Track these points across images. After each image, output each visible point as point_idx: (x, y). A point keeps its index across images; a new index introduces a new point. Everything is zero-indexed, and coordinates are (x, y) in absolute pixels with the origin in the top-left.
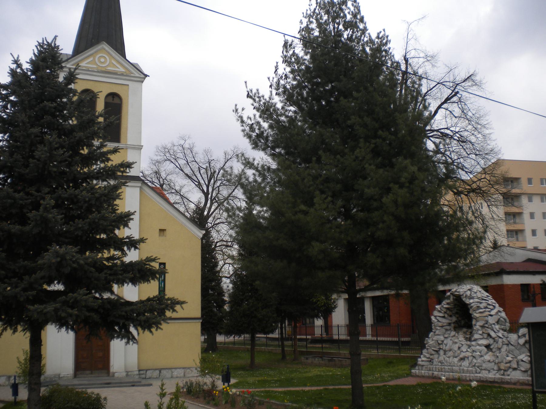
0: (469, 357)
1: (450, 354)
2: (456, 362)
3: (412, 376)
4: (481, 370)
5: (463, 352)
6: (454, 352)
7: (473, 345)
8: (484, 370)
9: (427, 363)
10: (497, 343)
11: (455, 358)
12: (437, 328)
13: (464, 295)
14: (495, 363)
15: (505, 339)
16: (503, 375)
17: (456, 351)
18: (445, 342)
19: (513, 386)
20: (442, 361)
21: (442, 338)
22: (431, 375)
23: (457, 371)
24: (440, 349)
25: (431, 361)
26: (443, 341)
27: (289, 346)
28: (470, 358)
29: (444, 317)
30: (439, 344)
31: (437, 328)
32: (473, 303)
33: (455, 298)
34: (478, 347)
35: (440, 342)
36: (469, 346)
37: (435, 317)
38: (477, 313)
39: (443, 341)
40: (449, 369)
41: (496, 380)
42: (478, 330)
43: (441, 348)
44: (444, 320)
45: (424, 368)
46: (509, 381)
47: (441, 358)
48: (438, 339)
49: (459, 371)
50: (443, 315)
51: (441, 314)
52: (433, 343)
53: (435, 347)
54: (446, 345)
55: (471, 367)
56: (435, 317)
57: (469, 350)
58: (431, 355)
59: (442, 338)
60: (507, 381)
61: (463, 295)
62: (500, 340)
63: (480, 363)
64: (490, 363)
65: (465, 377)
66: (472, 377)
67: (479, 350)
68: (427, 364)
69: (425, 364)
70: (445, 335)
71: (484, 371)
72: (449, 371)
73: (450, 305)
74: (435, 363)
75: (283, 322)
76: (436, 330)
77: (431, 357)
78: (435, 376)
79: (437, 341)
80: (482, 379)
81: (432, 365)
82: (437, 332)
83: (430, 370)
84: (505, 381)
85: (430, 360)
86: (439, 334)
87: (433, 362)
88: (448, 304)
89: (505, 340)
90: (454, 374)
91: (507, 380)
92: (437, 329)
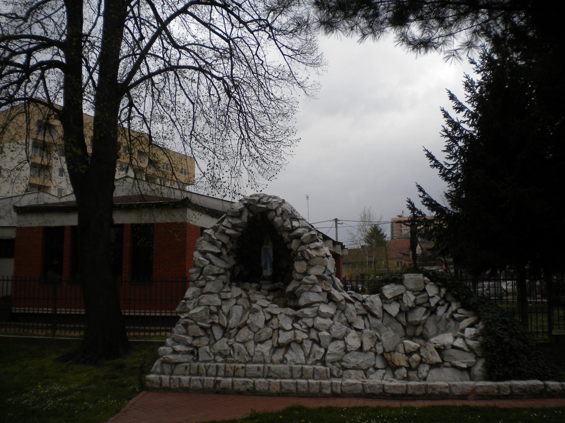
0: (304, 341)
1: (245, 334)
2: (267, 354)
3: (148, 389)
4: (344, 368)
5: (285, 330)
6: (255, 330)
7: (307, 316)
8: (353, 368)
9: (188, 356)
10: (343, 311)
11: (259, 345)
12: (209, 277)
13: (279, 211)
14: (376, 354)
15: (359, 303)
16: (408, 378)
17: (259, 329)
18: (225, 308)
19: (459, 403)
20: (225, 350)
21: (216, 300)
22: (211, 385)
23: (284, 374)
24: (213, 323)
25: (194, 352)
26: (219, 307)
27: (27, 310)
28: (308, 345)
29: (218, 255)
30: (212, 313)
31: (209, 277)
32: (299, 227)
33: (251, 215)
34: (319, 320)
35: (214, 309)
36: (296, 319)
37: (204, 253)
38: (311, 249)
39: (219, 307)
40: (259, 369)
41: (410, 392)
42: (314, 284)
43: (217, 321)
44: (219, 263)
45: (180, 369)
46: (447, 391)
47: (222, 344)
48: (210, 302)
49: (289, 373)
50: (219, 251)
51: (215, 247)
52: (201, 311)
53: (204, 321)
54: (228, 316)
55: (312, 364)
56: (204, 253)
57: (296, 325)
58: (194, 338)
59: (216, 300)
60: (440, 392)
61: (275, 210)
62: (350, 306)
63: (335, 354)
64: (362, 354)
65: (318, 387)
66: (339, 388)
67: (325, 325)
68: (186, 360)
69: (182, 360)
70: (221, 294)
71: (354, 371)
72: (260, 373)
73: (237, 231)
74: (203, 356)
75: (395, 3)
76: (207, 282)
77: (196, 342)
78: (225, 389)
79: (209, 306)
80: (368, 391)
81: (195, 361)
82: (209, 287)
83: (198, 374)
84: (436, 392)
85: (191, 349)
86: (212, 291)
87: (198, 355)
88: (234, 227)
89: (359, 305)
90: (283, 381)
91: (443, 390)
92: (210, 280)
